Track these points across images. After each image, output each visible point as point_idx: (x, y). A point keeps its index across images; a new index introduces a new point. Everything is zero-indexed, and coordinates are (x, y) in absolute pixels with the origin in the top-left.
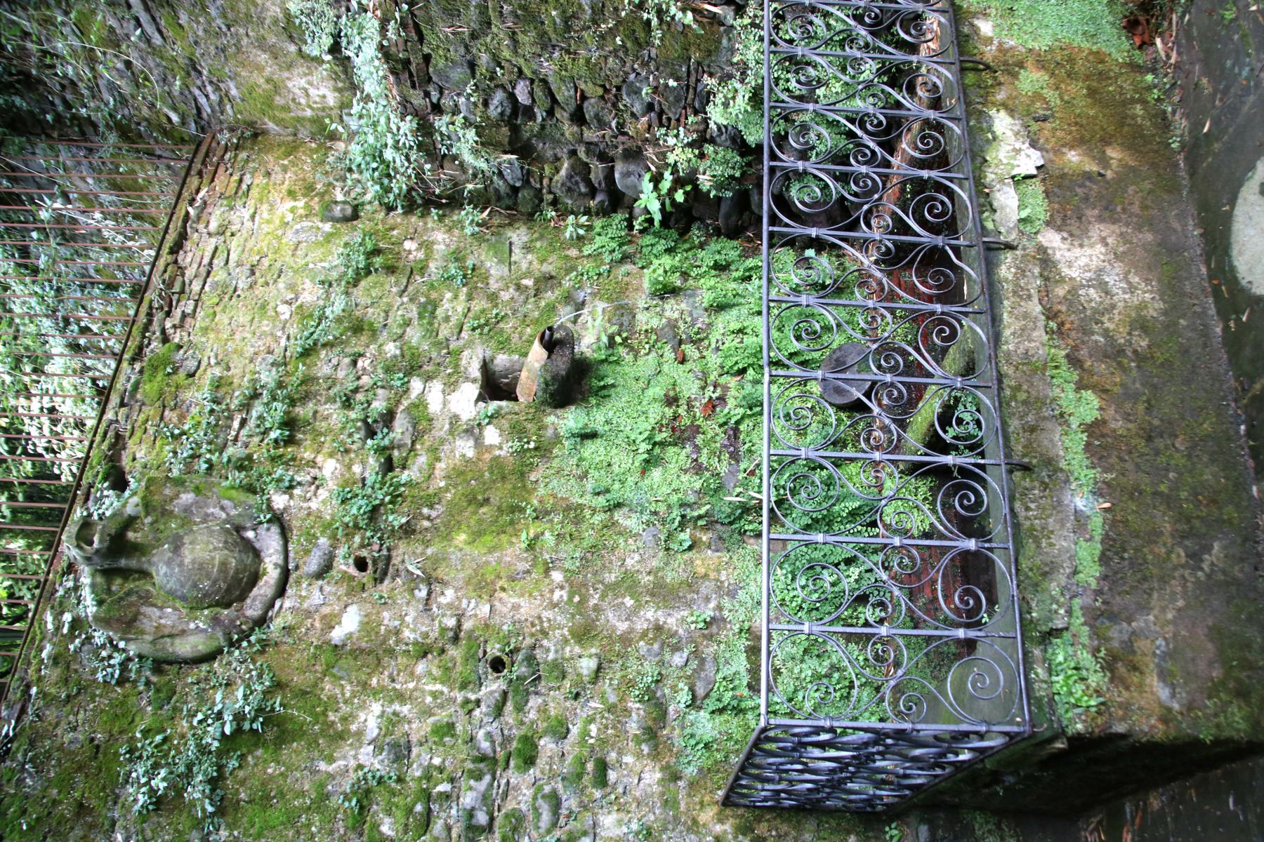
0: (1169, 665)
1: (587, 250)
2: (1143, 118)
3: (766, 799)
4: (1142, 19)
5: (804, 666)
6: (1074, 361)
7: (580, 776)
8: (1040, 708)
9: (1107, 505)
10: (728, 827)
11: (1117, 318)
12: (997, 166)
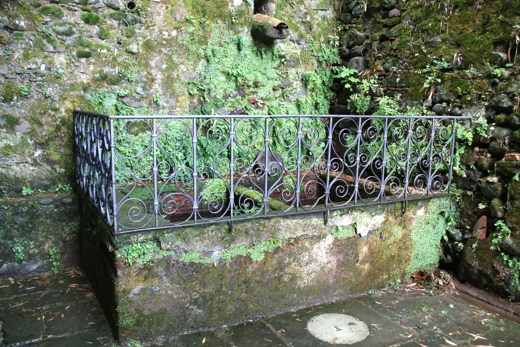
0: (148, 292)
1: (324, 46)
2: (382, 279)
3: (78, 129)
4: (424, 277)
5: (140, 146)
6: (277, 250)
7: (82, 45)
8: (126, 238)
9: (216, 265)
10: (64, 114)
11: (296, 268)
12: (361, 217)
